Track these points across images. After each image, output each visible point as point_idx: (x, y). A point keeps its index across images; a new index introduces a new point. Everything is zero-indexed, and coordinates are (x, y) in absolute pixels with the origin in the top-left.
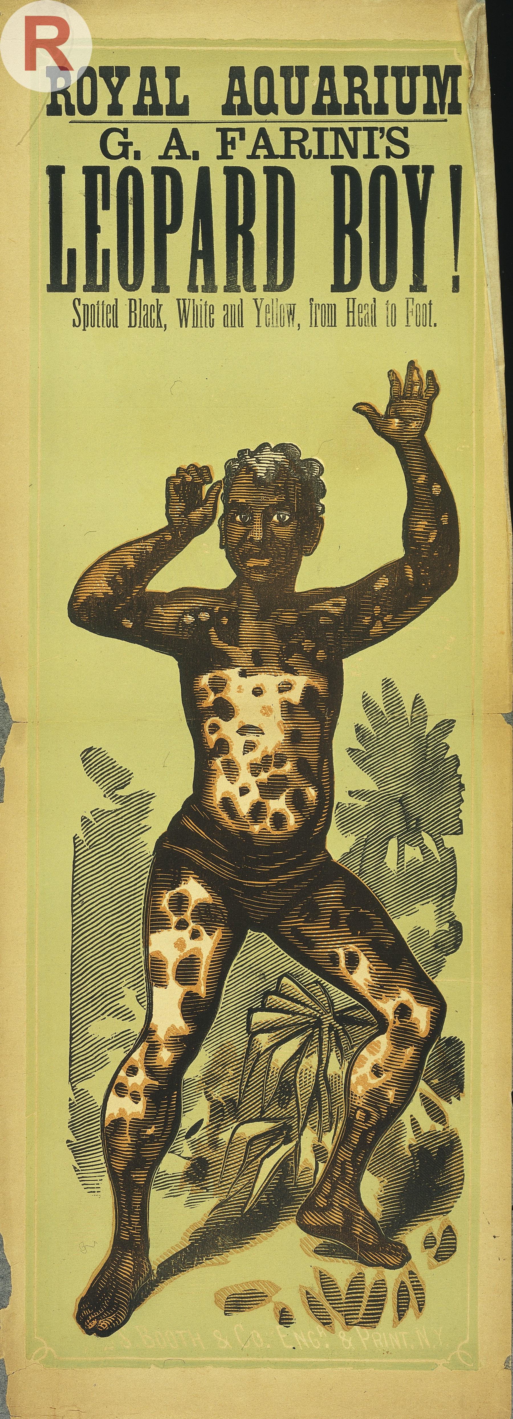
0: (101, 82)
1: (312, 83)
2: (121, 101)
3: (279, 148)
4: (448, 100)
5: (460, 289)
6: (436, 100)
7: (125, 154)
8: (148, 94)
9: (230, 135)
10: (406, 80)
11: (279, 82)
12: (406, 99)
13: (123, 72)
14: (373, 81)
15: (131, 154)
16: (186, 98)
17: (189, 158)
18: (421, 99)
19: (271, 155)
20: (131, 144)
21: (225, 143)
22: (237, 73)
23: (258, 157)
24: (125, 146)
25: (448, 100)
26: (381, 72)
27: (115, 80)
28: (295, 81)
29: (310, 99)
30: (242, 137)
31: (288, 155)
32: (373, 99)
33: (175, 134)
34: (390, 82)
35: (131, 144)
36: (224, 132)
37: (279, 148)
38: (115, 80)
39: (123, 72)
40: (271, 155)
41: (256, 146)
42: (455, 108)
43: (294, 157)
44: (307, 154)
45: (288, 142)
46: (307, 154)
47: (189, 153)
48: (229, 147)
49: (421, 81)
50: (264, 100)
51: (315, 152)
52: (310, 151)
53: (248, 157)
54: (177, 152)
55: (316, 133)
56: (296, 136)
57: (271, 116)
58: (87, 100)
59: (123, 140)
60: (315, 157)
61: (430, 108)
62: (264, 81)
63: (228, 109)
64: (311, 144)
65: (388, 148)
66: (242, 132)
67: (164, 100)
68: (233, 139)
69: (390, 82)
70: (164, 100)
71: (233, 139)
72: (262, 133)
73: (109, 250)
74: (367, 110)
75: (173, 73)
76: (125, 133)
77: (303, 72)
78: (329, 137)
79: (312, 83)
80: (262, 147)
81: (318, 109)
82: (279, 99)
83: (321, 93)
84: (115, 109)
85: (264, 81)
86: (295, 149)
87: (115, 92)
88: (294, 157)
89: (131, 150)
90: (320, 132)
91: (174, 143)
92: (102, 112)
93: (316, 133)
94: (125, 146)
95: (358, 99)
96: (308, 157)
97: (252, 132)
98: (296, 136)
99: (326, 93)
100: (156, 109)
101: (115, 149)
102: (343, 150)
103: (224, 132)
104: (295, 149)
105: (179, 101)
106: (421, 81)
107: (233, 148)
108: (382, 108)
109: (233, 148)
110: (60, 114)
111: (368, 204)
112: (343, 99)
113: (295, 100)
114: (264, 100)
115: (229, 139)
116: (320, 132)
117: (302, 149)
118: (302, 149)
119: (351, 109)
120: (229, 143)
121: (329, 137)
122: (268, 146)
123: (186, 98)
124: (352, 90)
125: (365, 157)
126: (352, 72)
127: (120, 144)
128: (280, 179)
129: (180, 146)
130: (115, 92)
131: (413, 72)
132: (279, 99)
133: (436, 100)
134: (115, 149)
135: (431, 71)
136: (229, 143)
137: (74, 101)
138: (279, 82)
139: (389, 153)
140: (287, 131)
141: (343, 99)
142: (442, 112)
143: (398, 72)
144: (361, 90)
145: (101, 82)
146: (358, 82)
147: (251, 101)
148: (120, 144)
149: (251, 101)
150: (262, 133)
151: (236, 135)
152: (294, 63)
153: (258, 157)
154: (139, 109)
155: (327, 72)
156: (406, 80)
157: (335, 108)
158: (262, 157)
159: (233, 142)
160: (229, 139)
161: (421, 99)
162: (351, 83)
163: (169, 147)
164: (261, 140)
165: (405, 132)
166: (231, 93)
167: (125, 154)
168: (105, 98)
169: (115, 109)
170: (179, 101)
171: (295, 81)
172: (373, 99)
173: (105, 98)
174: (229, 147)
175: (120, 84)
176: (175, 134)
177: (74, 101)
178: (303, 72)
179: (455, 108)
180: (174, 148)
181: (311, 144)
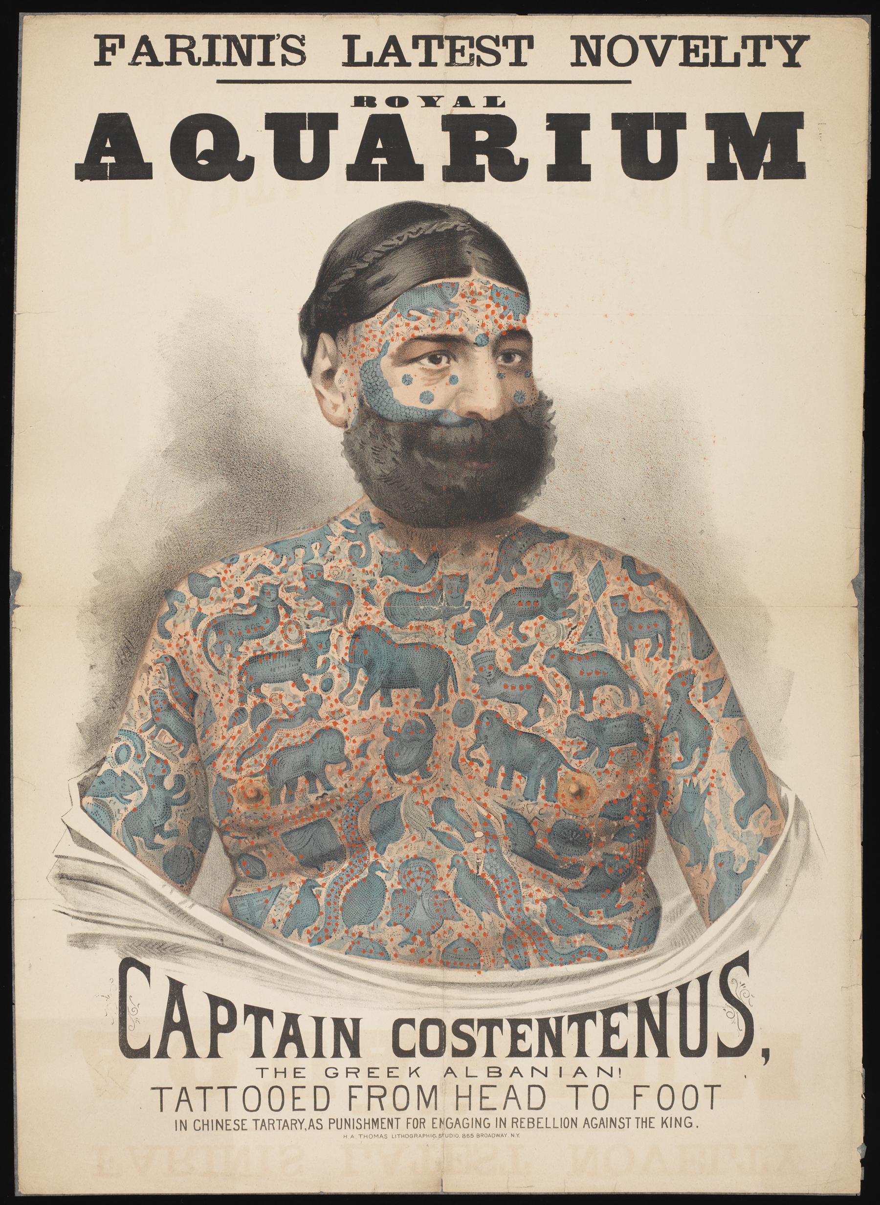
5: (805, 127)
9: (693, 43)
21: (103, 49)
23: (387, 65)
30: (122, 45)
36: (102, 38)
41: (138, 53)
43: (273, 64)
44: (196, 61)
45: (174, 50)
46: (196, 61)
51: (205, 58)
52: (200, 59)
54: (396, 60)
56: (182, 43)
60: (205, 64)
65: (284, 56)
66: (122, 38)
72: (144, 40)
73: (708, 116)
78: (221, 46)
96: (198, 64)
98: (182, 43)
103: (102, 38)
104: (182, 57)
107: (114, 54)
109: (114, 54)
115: (692, 47)
117: (191, 57)
118: (191, 57)
120: (692, 51)
121: (221, 46)
122: (151, 53)
125: (259, 64)
136: (458, 51)
139: (285, 61)
140: (173, 38)
150: (144, 40)
153: (387, 65)
160: (692, 47)
164: (392, 47)
165: (301, 40)
180: (143, 54)
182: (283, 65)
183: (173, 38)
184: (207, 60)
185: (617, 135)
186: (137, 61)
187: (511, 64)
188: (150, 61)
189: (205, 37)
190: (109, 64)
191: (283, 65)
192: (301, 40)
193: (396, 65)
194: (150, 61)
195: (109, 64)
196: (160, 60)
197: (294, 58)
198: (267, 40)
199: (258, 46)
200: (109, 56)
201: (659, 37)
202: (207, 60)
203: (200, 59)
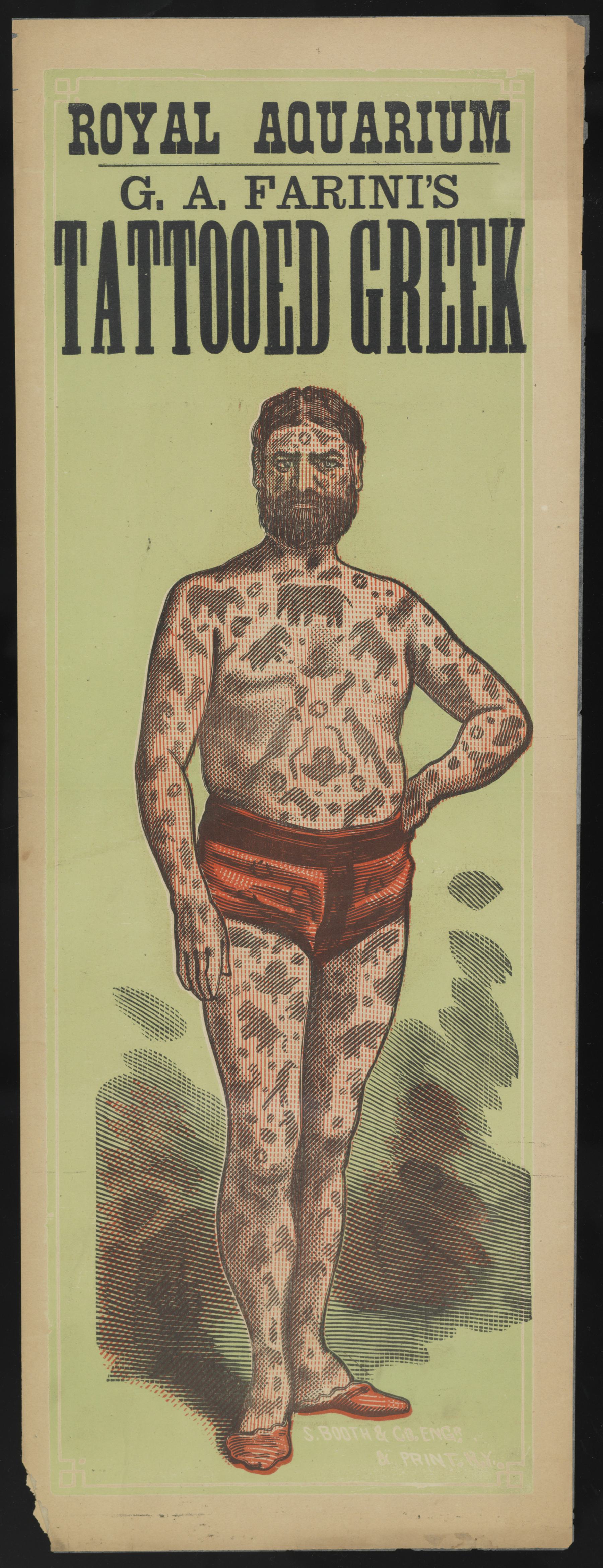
0: (126, 119)
1: (350, 120)
2: (147, 139)
3: (311, 197)
4: (496, 137)
6: (483, 137)
7: (147, 204)
8: (176, 131)
9: (259, 183)
10: (451, 117)
11: (315, 118)
12: (451, 136)
13: (150, 109)
14: (416, 118)
15: (154, 204)
16: (217, 136)
17: (215, 207)
18: (468, 136)
19: (303, 205)
20: (153, 193)
22: (270, 109)
24: (148, 195)
25: (496, 137)
26: (424, 108)
27: (141, 117)
28: (332, 118)
29: (349, 136)
30: (272, 186)
31: (321, 205)
32: (416, 137)
33: (201, 182)
34: (434, 118)
35: (153, 193)
36: (253, 180)
37: (311, 197)
38: (141, 117)
39: (150, 109)
40: (303, 205)
41: (287, 196)
42: (504, 146)
43: (327, 207)
44: (341, 203)
45: (321, 191)
46: (341, 203)
47: (215, 202)
48: (258, 196)
49: (468, 117)
50: (299, 137)
51: (351, 201)
52: (344, 201)
53: (279, 207)
54: (202, 202)
55: (352, 181)
56: (329, 185)
57: (306, 156)
58: (111, 139)
59: (144, 188)
60: (351, 207)
61: (476, 146)
62: (299, 117)
63: (261, 147)
64: (347, 193)
66: (272, 180)
67: (193, 137)
68: (263, 187)
69: (434, 118)
70: (193, 137)
71: (263, 187)
72: (294, 181)
74: (409, 147)
75: (202, 109)
76: (147, 182)
77: (340, 108)
78: (367, 187)
79: (350, 120)
80: (293, 197)
81: (357, 147)
82: (315, 136)
83: (360, 130)
84: (141, 147)
85: (299, 117)
86: (328, 199)
87: (141, 129)
88: (327, 207)
89: (154, 199)
90: (357, 180)
91: (199, 192)
92: (127, 151)
93: (352, 181)
94: (148, 195)
95: (400, 136)
97: (282, 184)
98: (329, 185)
99: (366, 130)
100: (184, 147)
101: (136, 198)
102: (383, 199)
103: (253, 180)
104: (328, 199)
105: (209, 138)
106: (468, 117)
107: (263, 197)
108: (426, 146)
109: (263, 197)
110: (83, 153)
111: (382, 326)
112: (383, 137)
113: (332, 137)
114: (299, 137)
115: (258, 188)
116: (357, 180)
119: (393, 146)
121: (367, 187)
122: (299, 195)
123: (217, 136)
124: (394, 127)
126: (393, 108)
127: (142, 193)
128: (314, 233)
129: (206, 196)
130: (141, 129)
131: (459, 107)
132: (315, 136)
133: (483, 137)
134: (136, 198)
135: (478, 107)
137: (98, 139)
138: (315, 118)
139: (437, 203)
140: (320, 180)
141: (383, 137)
142: (489, 150)
143: (442, 108)
144: (403, 127)
145: (126, 119)
146: (399, 118)
147: (285, 138)
148: (142, 193)
149: (285, 138)
150: (294, 181)
151: (266, 183)
152: (330, 98)
153: (289, 207)
154: (167, 147)
155: (366, 109)
156: (451, 117)
157: (374, 146)
158: (293, 207)
159: (262, 192)
160: (258, 188)
161: (468, 136)
162: (392, 119)
163: (194, 196)
165: (454, 180)
166: (264, 130)
167: (147, 204)
168: (130, 135)
169: (141, 147)
170: (209, 138)
171: (332, 118)
172: (416, 137)
173: (130, 135)
174: (258, 196)
175: (147, 121)
176: (201, 182)
177: (98, 139)
178: (340, 108)
179: (504, 146)
180: (199, 197)
181: (347, 193)
182: (435, 206)
183: (320, 180)
184: (352, 203)
185: (124, 345)
186: (194, 204)
187: (409, 206)
188: (298, 203)
189: (350, 177)
190: (260, 207)
191: (435, 206)
192: (454, 180)
193: (203, 207)
194: (298, 203)
195: (260, 207)
196: (308, 203)
197: (447, 199)
198: (415, 179)
199: (405, 187)
200: (259, 201)
201: (405, 177)
202: (352, 203)
203: (344, 201)
